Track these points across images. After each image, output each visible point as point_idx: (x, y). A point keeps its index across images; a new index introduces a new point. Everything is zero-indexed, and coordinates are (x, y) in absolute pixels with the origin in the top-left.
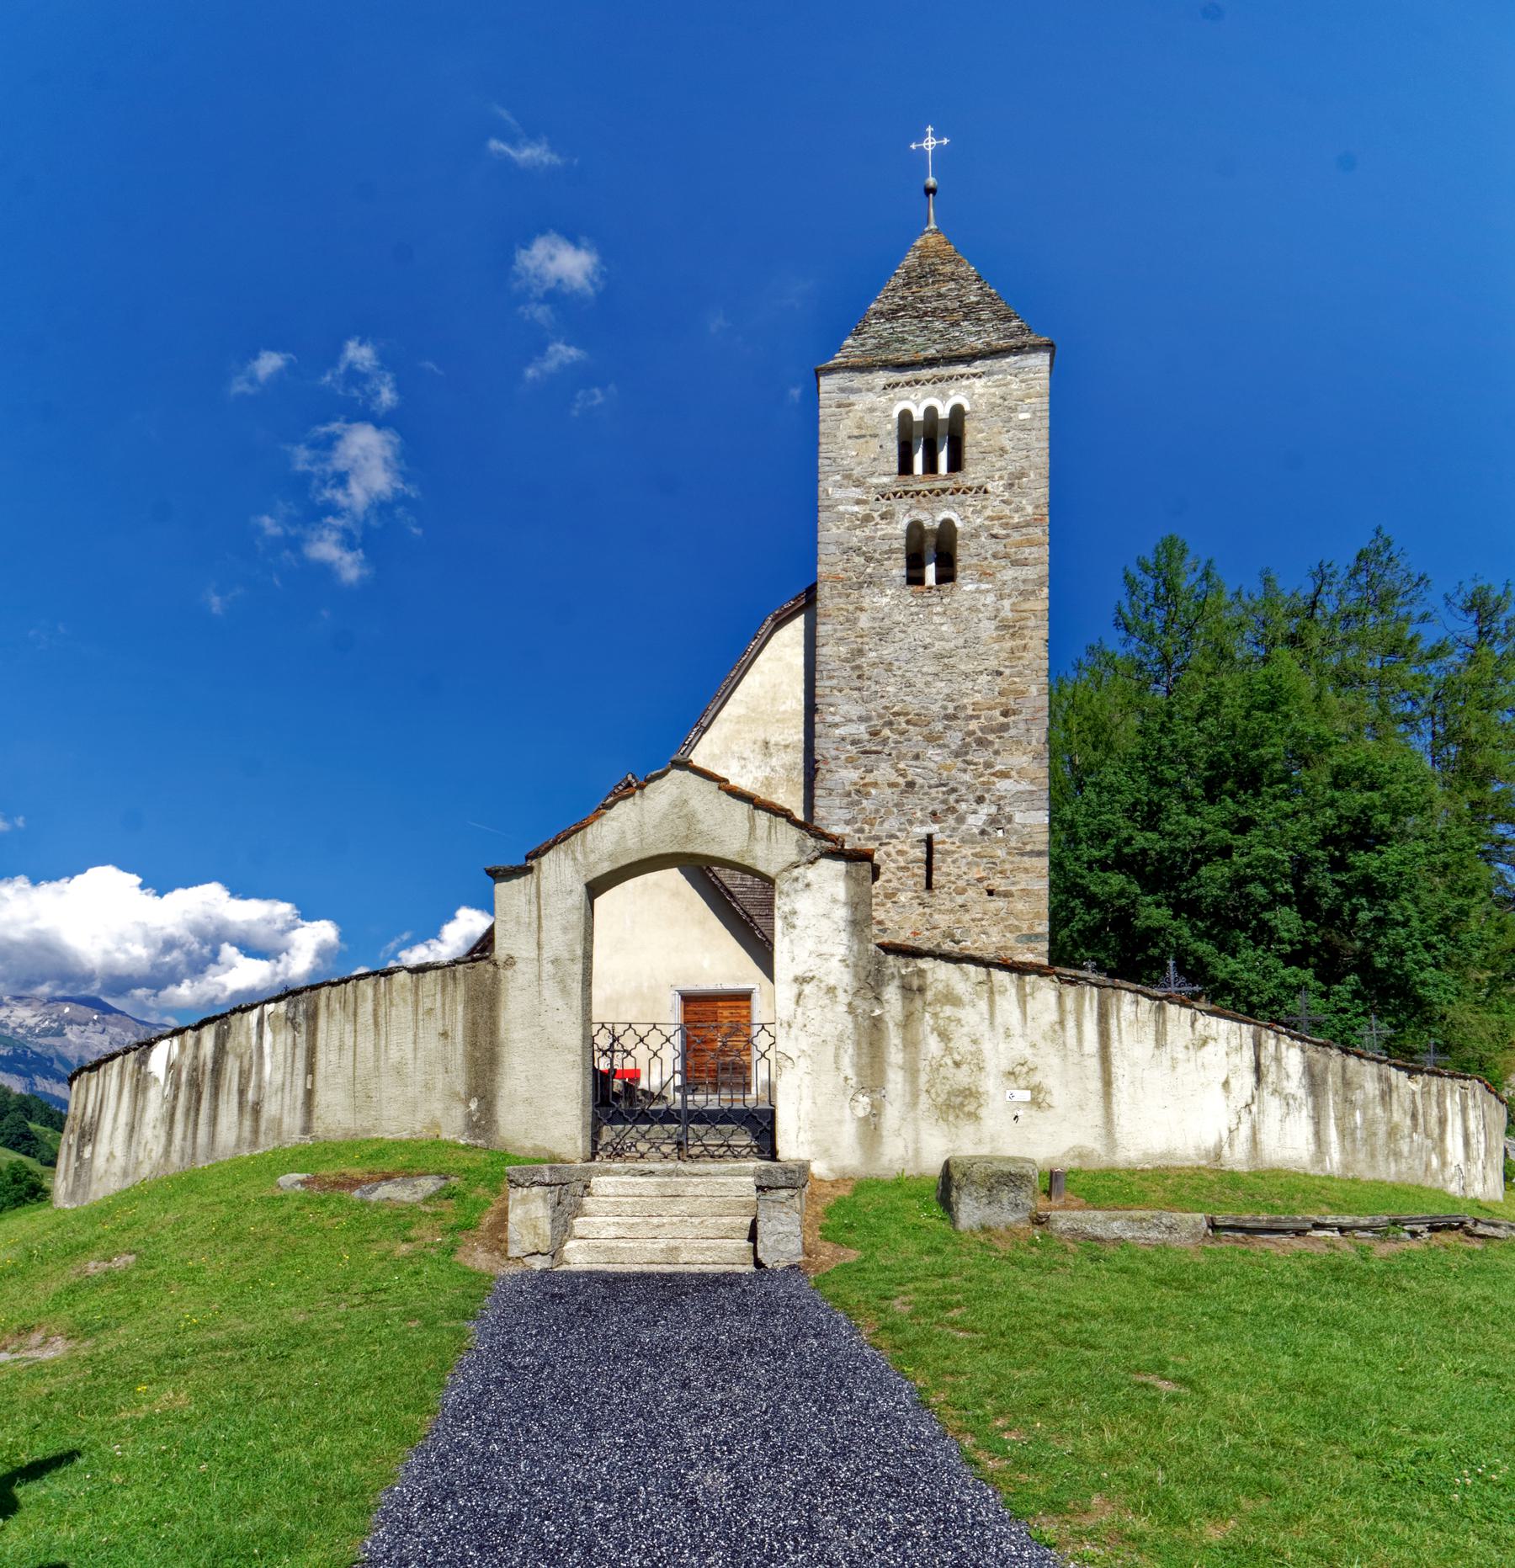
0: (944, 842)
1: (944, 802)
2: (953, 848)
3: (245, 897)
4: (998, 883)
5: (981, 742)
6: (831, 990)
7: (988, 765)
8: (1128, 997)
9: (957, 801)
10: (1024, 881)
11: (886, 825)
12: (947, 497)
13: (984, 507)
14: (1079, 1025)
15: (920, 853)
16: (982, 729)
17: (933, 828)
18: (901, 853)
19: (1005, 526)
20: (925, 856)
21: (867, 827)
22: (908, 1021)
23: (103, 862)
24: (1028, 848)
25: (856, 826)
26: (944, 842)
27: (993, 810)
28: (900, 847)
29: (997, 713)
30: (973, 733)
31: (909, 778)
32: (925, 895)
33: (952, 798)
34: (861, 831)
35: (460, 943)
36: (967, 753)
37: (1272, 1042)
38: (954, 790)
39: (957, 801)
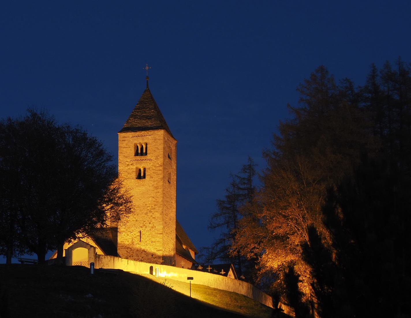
0: (143, 232)
1: (143, 224)
2: (145, 233)
3: (118, 269)
4: (153, 240)
5: (150, 212)
6: (92, 258)
7: (151, 216)
8: (116, 258)
9: (146, 224)
10: (158, 239)
11: (132, 229)
12: (144, 161)
13: (151, 163)
14: (112, 260)
15: (139, 234)
16: (150, 209)
17: (141, 229)
18: (134, 234)
19: (155, 167)
20: (140, 235)
21: (128, 229)
22: (99, 260)
23: (124, 271)
24: (159, 233)
25: (126, 229)
26: (143, 232)
27: (152, 225)
28: (134, 233)
29: (153, 205)
30: (149, 210)
31: (136, 219)
32: (139, 243)
33: (145, 223)
34: (127, 230)
35: (173, 246)
36: (147, 214)
37: (130, 261)
38: (145, 221)
39: (146, 224)
